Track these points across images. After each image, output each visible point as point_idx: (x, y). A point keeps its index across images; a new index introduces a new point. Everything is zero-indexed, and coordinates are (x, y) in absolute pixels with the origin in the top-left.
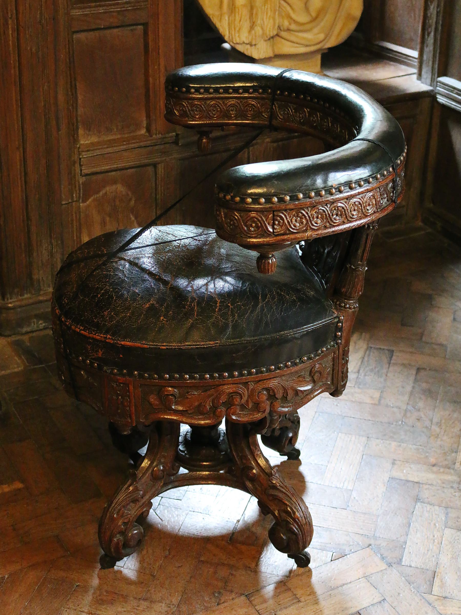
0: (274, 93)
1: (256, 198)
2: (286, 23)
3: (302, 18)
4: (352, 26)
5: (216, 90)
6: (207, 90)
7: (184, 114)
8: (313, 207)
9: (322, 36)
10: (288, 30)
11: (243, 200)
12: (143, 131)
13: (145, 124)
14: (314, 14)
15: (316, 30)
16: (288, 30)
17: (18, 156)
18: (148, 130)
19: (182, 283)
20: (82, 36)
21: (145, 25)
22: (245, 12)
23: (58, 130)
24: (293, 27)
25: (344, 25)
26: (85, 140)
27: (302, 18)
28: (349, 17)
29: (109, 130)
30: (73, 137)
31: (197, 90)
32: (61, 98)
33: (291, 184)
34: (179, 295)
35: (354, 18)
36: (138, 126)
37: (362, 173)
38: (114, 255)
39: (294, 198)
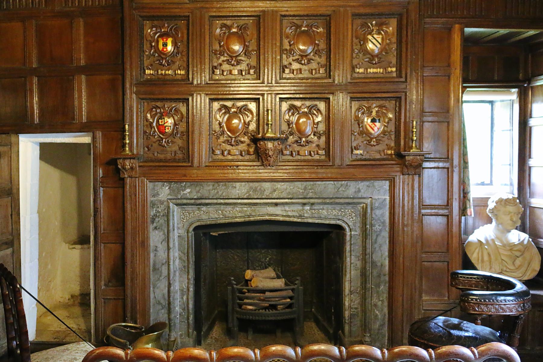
0: (488, 281)
1: (472, 299)
2: (505, 269)
3: (512, 267)
4: (535, 273)
5: (468, 278)
6: (464, 277)
7: (456, 284)
8: (492, 305)
9: (521, 275)
10: (506, 271)
11: (468, 299)
12: (446, 298)
13: (447, 296)
14: (517, 267)
15: (518, 272)
16: (506, 271)
17: (401, 298)
18: (448, 298)
19: (452, 331)
20: (426, 263)
21: (448, 262)
22: (488, 263)
23: (416, 292)
24: (508, 270)
25: (531, 273)
26: (425, 297)
27: (512, 267)
28: (534, 270)
29: (433, 296)
30: (421, 297)
31: (461, 277)
32: (417, 282)
33: (484, 297)
34: (450, 334)
35: (536, 271)
36: (444, 296)
37: (511, 298)
38: (429, 321)
39: (485, 301)
